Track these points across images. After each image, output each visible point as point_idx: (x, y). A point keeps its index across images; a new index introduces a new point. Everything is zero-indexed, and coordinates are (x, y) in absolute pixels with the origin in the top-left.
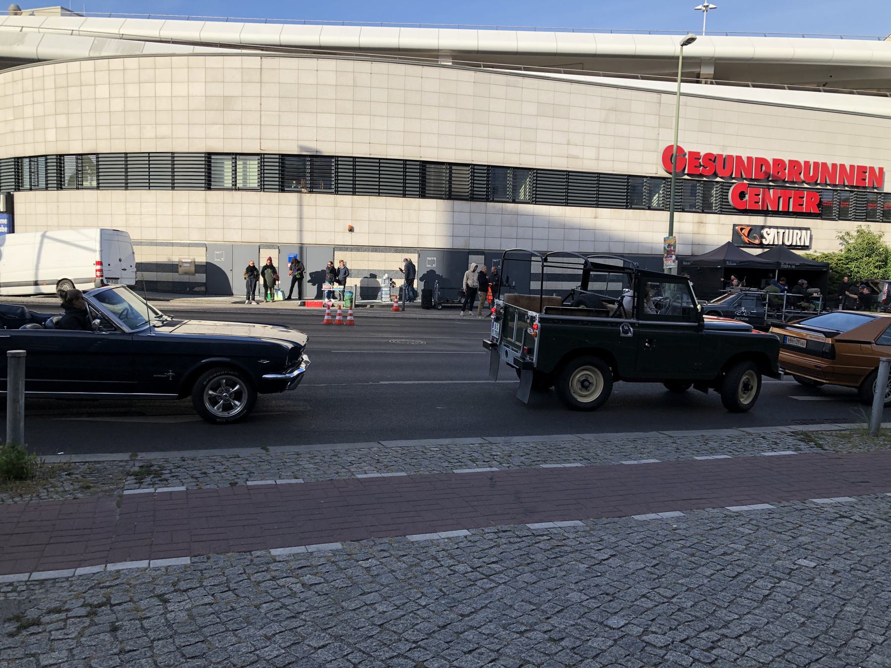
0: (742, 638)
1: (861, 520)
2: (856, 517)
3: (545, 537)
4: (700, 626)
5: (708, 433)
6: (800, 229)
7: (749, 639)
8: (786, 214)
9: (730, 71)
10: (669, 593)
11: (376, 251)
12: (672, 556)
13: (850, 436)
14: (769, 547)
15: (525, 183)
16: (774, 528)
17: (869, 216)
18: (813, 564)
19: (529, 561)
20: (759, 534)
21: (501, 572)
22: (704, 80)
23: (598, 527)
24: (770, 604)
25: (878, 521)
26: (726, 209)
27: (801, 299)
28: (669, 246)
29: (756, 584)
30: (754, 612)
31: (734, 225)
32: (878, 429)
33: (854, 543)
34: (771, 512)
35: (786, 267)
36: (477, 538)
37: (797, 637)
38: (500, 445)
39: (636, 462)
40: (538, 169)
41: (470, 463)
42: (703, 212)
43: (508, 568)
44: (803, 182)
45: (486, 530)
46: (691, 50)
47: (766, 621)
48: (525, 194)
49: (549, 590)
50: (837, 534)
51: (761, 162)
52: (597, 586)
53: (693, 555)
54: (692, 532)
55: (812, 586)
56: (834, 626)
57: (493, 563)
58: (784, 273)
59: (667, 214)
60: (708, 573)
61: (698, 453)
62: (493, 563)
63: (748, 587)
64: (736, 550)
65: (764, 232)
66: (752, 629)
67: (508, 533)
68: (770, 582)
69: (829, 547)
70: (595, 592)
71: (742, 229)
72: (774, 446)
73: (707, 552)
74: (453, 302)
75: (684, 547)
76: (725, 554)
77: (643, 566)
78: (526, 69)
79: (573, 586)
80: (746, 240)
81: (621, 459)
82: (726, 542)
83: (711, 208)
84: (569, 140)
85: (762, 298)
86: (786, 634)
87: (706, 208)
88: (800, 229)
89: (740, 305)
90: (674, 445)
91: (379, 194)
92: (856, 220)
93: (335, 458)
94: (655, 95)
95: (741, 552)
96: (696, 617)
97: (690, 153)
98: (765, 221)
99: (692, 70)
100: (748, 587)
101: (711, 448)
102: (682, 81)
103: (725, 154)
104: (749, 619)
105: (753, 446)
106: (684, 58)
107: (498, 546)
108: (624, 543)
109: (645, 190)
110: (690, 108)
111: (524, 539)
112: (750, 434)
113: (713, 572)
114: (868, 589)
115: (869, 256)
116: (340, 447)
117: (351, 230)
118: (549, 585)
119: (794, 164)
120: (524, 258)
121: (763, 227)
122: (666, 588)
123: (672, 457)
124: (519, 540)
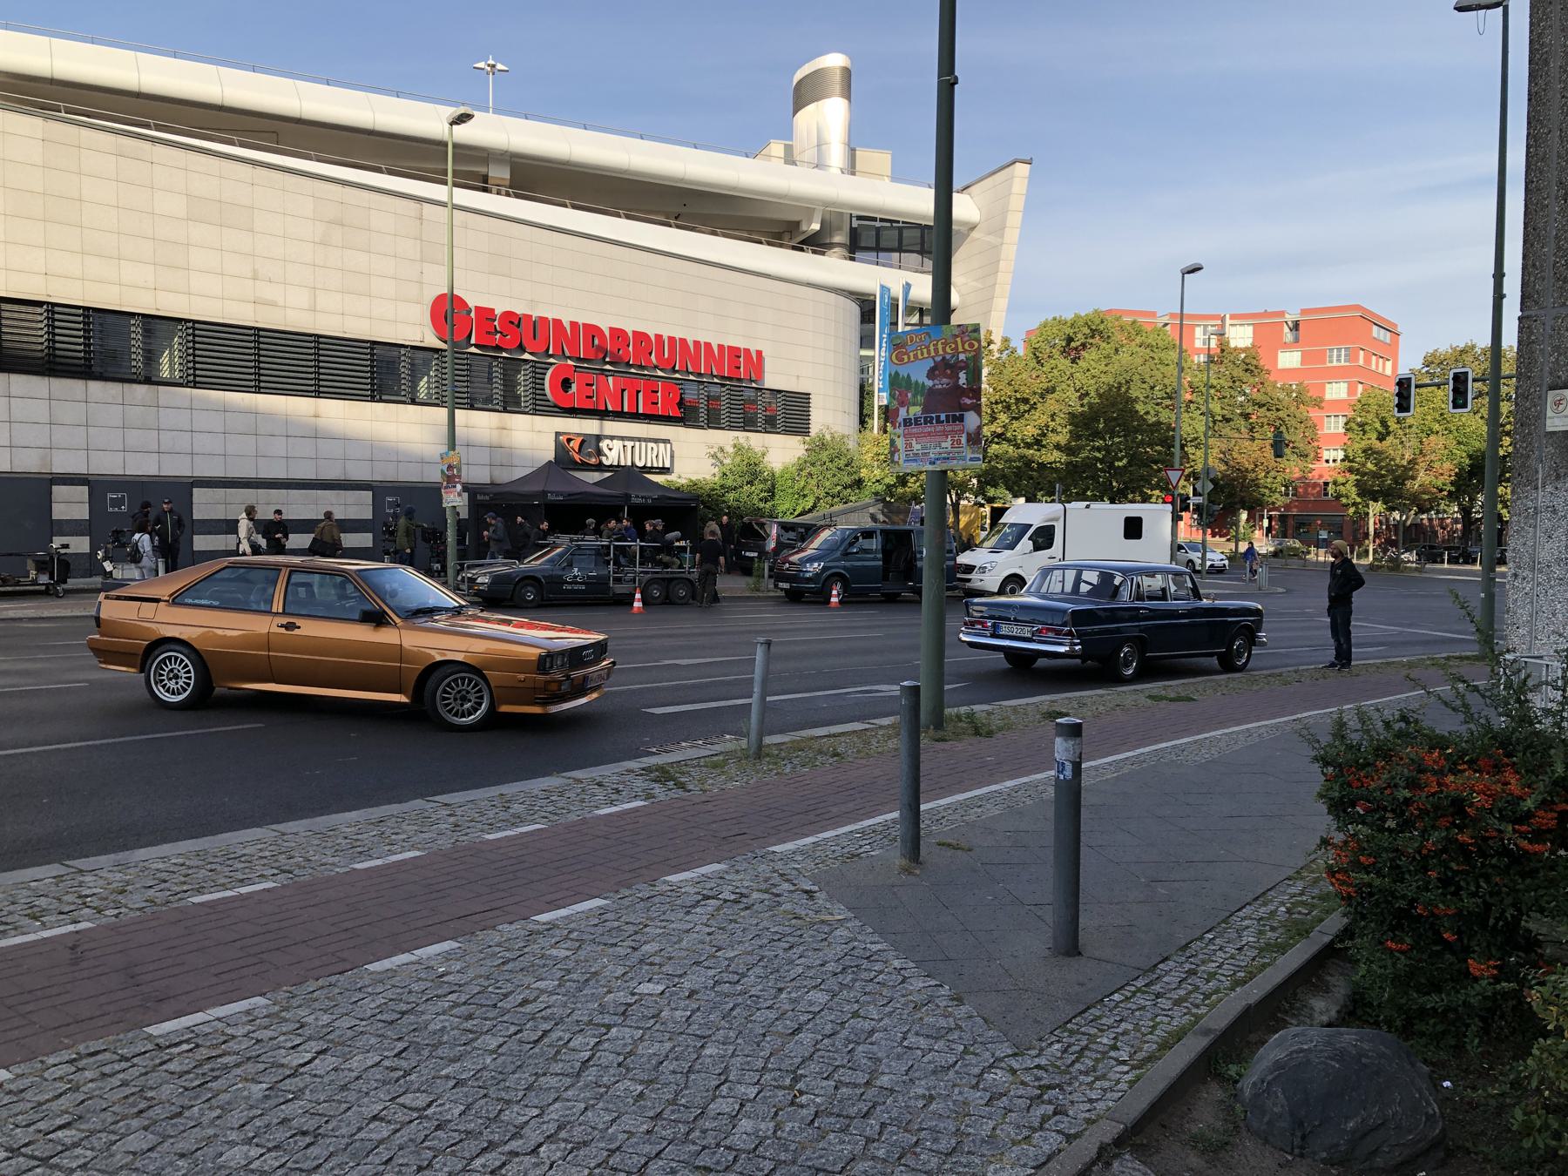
0: (542, 1149)
1: (733, 897)
2: (726, 895)
3: (185, 1047)
4: (473, 1146)
5: (509, 789)
6: (656, 441)
7: (553, 1147)
8: (634, 416)
9: (535, 178)
10: (421, 1100)
12: (432, 1027)
13: (725, 762)
14: (596, 973)
15: (171, 347)
16: (606, 939)
17: (748, 424)
18: (661, 988)
19: (143, 1105)
20: (582, 954)
21: (75, 1145)
22: (495, 189)
23: (295, 1002)
24: (591, 1074)
25: (755, 895)
26: (541, 407)
27: (658, 550)
28: (450, 467)
29: (571, 1044)
30: (565, 1095)
31: (558, 434)
32: (760, 746)
33: (721, 938)
34: (603, 911)
35: (640, 501)
36: (21, 1084)
37: (628, 1122)
38: (103, 874)
39: (379, 862)
40: (195, 322)
41: (27, 921)
42: (505, 411)
43: (92, 1132)
44: (656, 367)
45: (51, 1060)
46: (463, 133)
47: (583, 1105)
48: (172, 369)
49: (182, 1156)
50: (697, 928)
51: (592, 331)
52: (284, 1121)
53: (470, 1017)
54: (471, 974)
55: (657, 1026)
56: (686, 1087)
57: (60, 1128)
58: (640, 514)
59: (441, 414)
60: (494, 1043)
61: (492, 827)
62: (60, 1128)
63: (558, 1052)
64: (542, 991)
65: (604, 445)
66: (560, 1128)
67: (99, 1057)
68: (594, 1036)
69: (684, 954)
70: (280, 1135)
71: (569, 440)
72: (614, 797)
73: (495, 1006)
74: (18, 583)
75: (456, 1005)
76: (525, 1002)
77: (377, 1059)
78: (158, 128)
79: (233, 1136)
80: (577, 457)
81: (353, 860)
82: (528, 980)
83: (518, 404)
84: (255, 271)
85: (602, 552)
86: (614, 1121)
87: (510, 404)
88: (656, 441)
89: (570, 565)
90: (452, 819)
92: (731, 428)
94: (412, 204)
95: (551, 994)
96: (468, 1132)
97: (477, 308)
98: (601, 427)
99: (474, 168)
100: (558, 1052)
101: (513, 815)
102: (455, 185)
103: (535, 314)
104: (555, 1112)
105: (582, 801)
106: (455, 146)
107: (76, 1089)
108: (347, 1022)
109: (404, 371)
110: (473, 233)
111: (135, 1060)
112: (579, 781)
113: (501, 1040)
114: (738, 1010)
115: (750, 483)
118: (182, 1146)
119: (640, 337)
120: (184, 488)
121: (599, 438)
122: (418, 1090)
123: (445, 843)
124: (124, 1065)
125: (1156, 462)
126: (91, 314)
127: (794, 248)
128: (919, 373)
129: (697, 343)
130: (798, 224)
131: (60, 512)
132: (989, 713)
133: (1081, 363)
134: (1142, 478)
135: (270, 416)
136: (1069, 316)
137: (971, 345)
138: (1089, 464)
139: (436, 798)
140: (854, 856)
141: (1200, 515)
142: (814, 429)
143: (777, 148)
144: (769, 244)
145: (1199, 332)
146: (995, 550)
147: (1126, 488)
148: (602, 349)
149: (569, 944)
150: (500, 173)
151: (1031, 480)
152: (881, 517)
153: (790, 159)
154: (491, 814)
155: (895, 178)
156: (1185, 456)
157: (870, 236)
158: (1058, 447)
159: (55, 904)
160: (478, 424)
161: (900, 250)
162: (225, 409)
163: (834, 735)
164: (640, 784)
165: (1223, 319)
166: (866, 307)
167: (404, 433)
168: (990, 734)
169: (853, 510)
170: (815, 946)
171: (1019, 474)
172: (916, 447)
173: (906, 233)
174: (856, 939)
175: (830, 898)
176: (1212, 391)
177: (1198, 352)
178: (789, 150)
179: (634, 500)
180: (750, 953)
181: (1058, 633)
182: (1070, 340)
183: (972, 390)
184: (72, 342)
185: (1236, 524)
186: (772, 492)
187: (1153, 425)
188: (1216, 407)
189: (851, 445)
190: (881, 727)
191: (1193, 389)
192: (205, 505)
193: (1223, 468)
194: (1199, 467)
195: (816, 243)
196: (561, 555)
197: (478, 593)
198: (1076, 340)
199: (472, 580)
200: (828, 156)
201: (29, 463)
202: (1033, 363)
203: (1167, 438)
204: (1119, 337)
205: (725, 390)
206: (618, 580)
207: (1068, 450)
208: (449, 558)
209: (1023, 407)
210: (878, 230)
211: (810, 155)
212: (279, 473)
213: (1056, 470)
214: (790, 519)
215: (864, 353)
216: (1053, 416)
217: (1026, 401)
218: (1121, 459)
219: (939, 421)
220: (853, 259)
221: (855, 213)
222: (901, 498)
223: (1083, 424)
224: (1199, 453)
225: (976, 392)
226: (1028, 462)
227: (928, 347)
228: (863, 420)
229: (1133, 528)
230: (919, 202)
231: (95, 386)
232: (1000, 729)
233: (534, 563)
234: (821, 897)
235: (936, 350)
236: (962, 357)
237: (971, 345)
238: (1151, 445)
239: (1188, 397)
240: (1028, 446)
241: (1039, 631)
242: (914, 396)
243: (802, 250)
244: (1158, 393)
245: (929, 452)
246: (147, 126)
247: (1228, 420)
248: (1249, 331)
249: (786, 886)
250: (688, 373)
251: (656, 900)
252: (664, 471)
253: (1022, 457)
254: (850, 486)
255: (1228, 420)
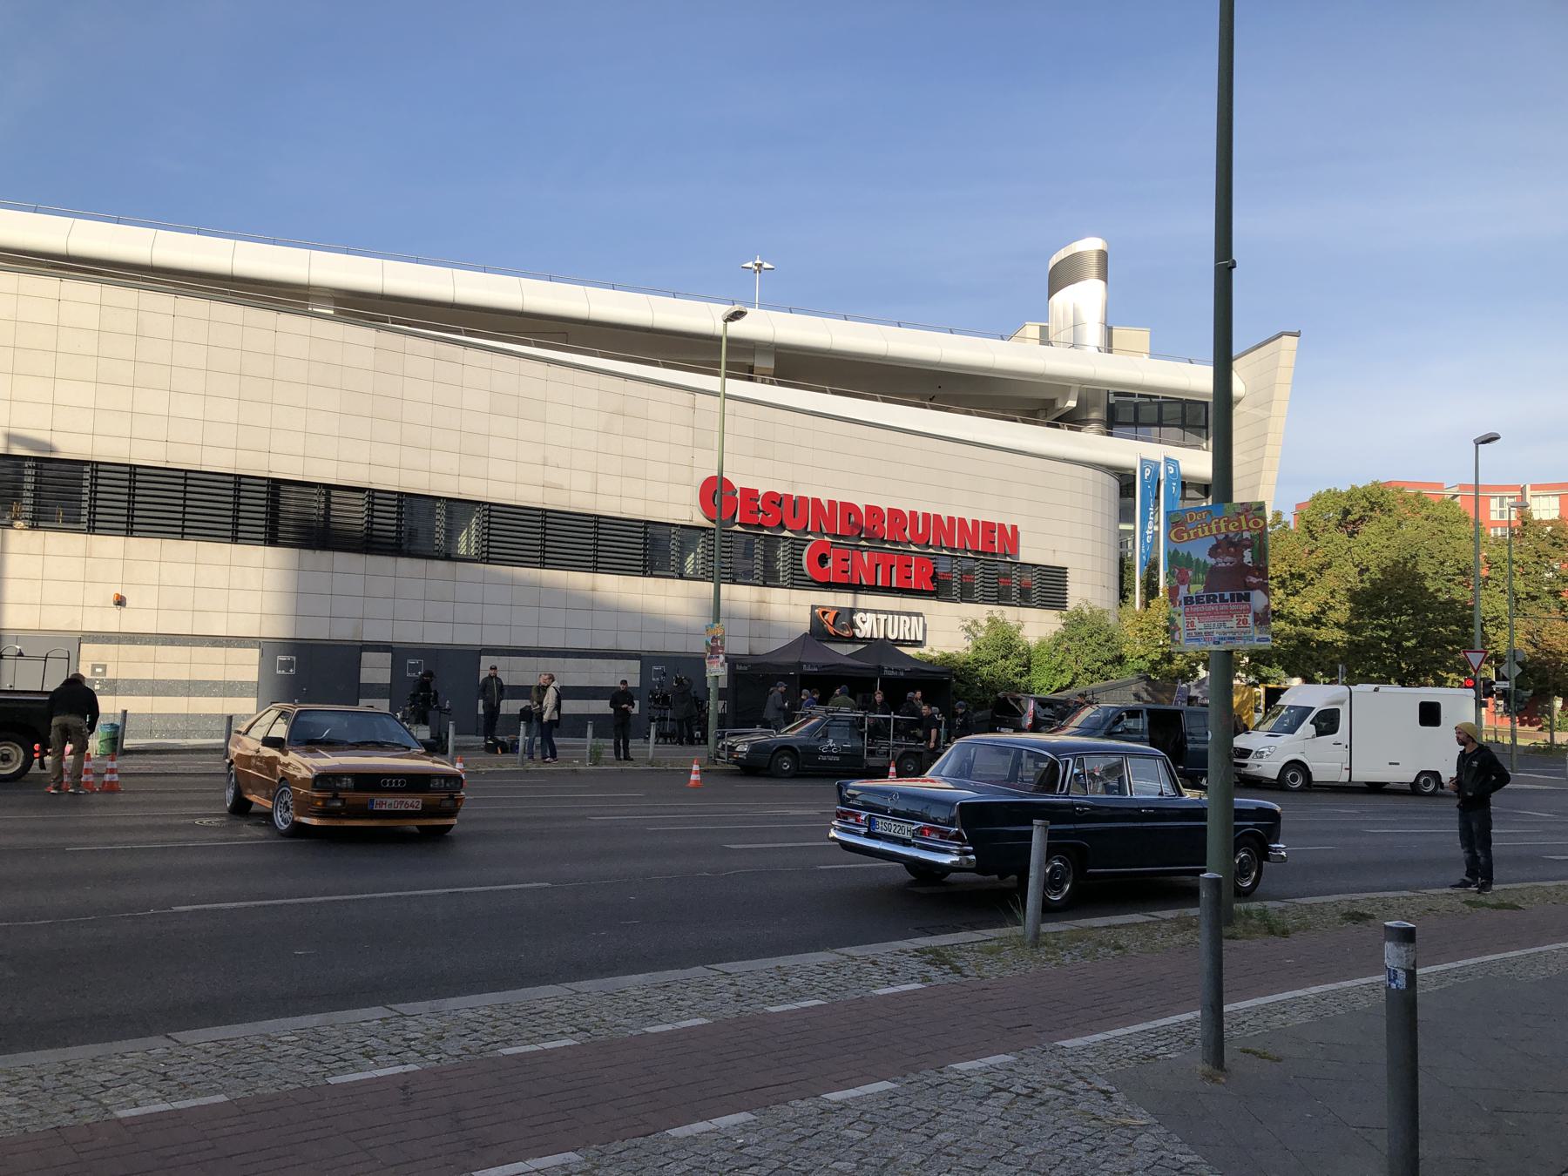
1: (1025, 1091)
2: (1017, 1088)
6: (909, 614)
11: (172, 643)
15: (469, 527)
16: (899, 1124)
17: (1002, 598)
20: (877, 1138)
25: (1049, 1092)
26: (799, 581)
28: (714, 639)
31: (814, 607)
34: (892, 1096)
39: (669, 1027)
40: (98, 463)
42: (765, 585)
46: (738, 329)
51: (849, 508)
59: (707, 588)
65: (857, 618)
71: (824, 613)
72: (890, 977)
78: (468, 333)
80: (831, 630)
82: (825, 1160)
87: (769, 579)
88: (909, 614)
89: (826, 737)
91: (183, 536)
92: (985, 602)
93: (68, 1079)
94: (685, 394)
98: (855, 601)
99: (745, 359)
101: (792, 989)
102: (728, 376)
103: (795, 494)
106: (729, 340)
109: (674, 547)
112: (853, 958)
115: (1005, 657)
116: (78, 1054)
117: (120, 602)
121: (852, 611)
123: (730, 1012)
125: (1451, 643)
126: (405, 500)
127: (1049, 425)
128: (1200, 552)
129: (951, 519)
130: (1053, 402)
131: (367, 676)
132: (1281, 911)
133: (1359, 537)
134: (1435, 660)
135: (552, 589)
136: (1344, 488)
137: (1256, 524)
138: (1373, 644)
139: (717, 966)
140: (1149, 1057)
141: (1507, 701)
142: (1072, 603)
143: (1032, 330)
144: (1024, 422)
145: (1494, 504)
146: (1273, 733)
147: (1417, 670)
148: (858, 525)
149: (863, 1126)
150: (765, 363)
151: (1306, 659)
152: (1145, 696)
153: (1045, 340)
154: (771, 985)
155: (1153, 355)
156: (1485, 636)
157: (1127, 411)
158: (1338, 625)
159: (384, 1045)
160: (740, 596)
161: (1160, 424)
162: (513, 583)
163: (1115, 927)
164: (915, 965)
165: (1523, 490)
166: (1125, 481)
167: (669, 602)
168: (1285, 933)
169: (1114, 687)
170: (1119, 1150)
171: (1295, 654)
172: (1199, 626)
173: (1166, 408)
174: (1163, 1148)
175: (1129, 1101)
176: (1514, 567)
177: (1495, 525)
178: (1044, 331)
179: (887, 673)
180: (1052, 1152)
181: (944, 835)
182: (1347, 512)
183: (1258, 569)
184: (387, 523)
185: (1550, 712)
186: (1027, 667)
187: (1446, 603)
188: (1519, 585)
189: (1112, 620)
190: (1164, 920)
191: (1491, 564)
192: (513, 672)
193: (1532, 650)
194: (1503, 649)
195: (1072, 421)
196: (815, 727)
197: (737, 762)
198: (1355, 511)
199: (732, 748)
200: (1077, 336)
201: (343, 631)
202: (1306, 537)
203: (1463, 618)
204: (1402, 510)
205: (978, 563)
206: (872, 753)
207: (1349, 627)
208: (710, 726)
209: (1299, 584)
210: (1136, 405)
211: (1067, 335)
212: (557, 643)
213: (1337, 649)
214: (1046, 695)
215: (1123, 527)
216: (1333, 593)
217: (1301, 576)
218: (1408, 639)
219: (1222, 600)
220: (1110, 434)
221: (1112, 389)
222: (1167, 675)
223: (1366, 601)
224: (1500, 633)
225: (1263, 572)
226: (1305, 641)
227: (1209, 525)
228: (1124, 594)
229: (1430, 714)
230: (1198, 379)
231: (404, 563)
232: (1297, 929)
233: (792, 734)
234: (1119, 1099)
235: (1218, 528)
236: (1246, 535)
237: (1256, 524)
238: (1444, 625)
239: (1484, 573)
240: (1306, 623)
241: (921, 831)
242: (1196, 573)
243: (1057, 426)
244: (1449, 568)
245: (1203, 633)
246: (458, 332)
247: (1534, 598)
248: (1554, 502)
249: (1080, 1084)
250: (942, 548)
251: (946, 1087)
252: (916, 643)
253: (1299, 635)
254: (1111, 662)
255: (1534, 598)
